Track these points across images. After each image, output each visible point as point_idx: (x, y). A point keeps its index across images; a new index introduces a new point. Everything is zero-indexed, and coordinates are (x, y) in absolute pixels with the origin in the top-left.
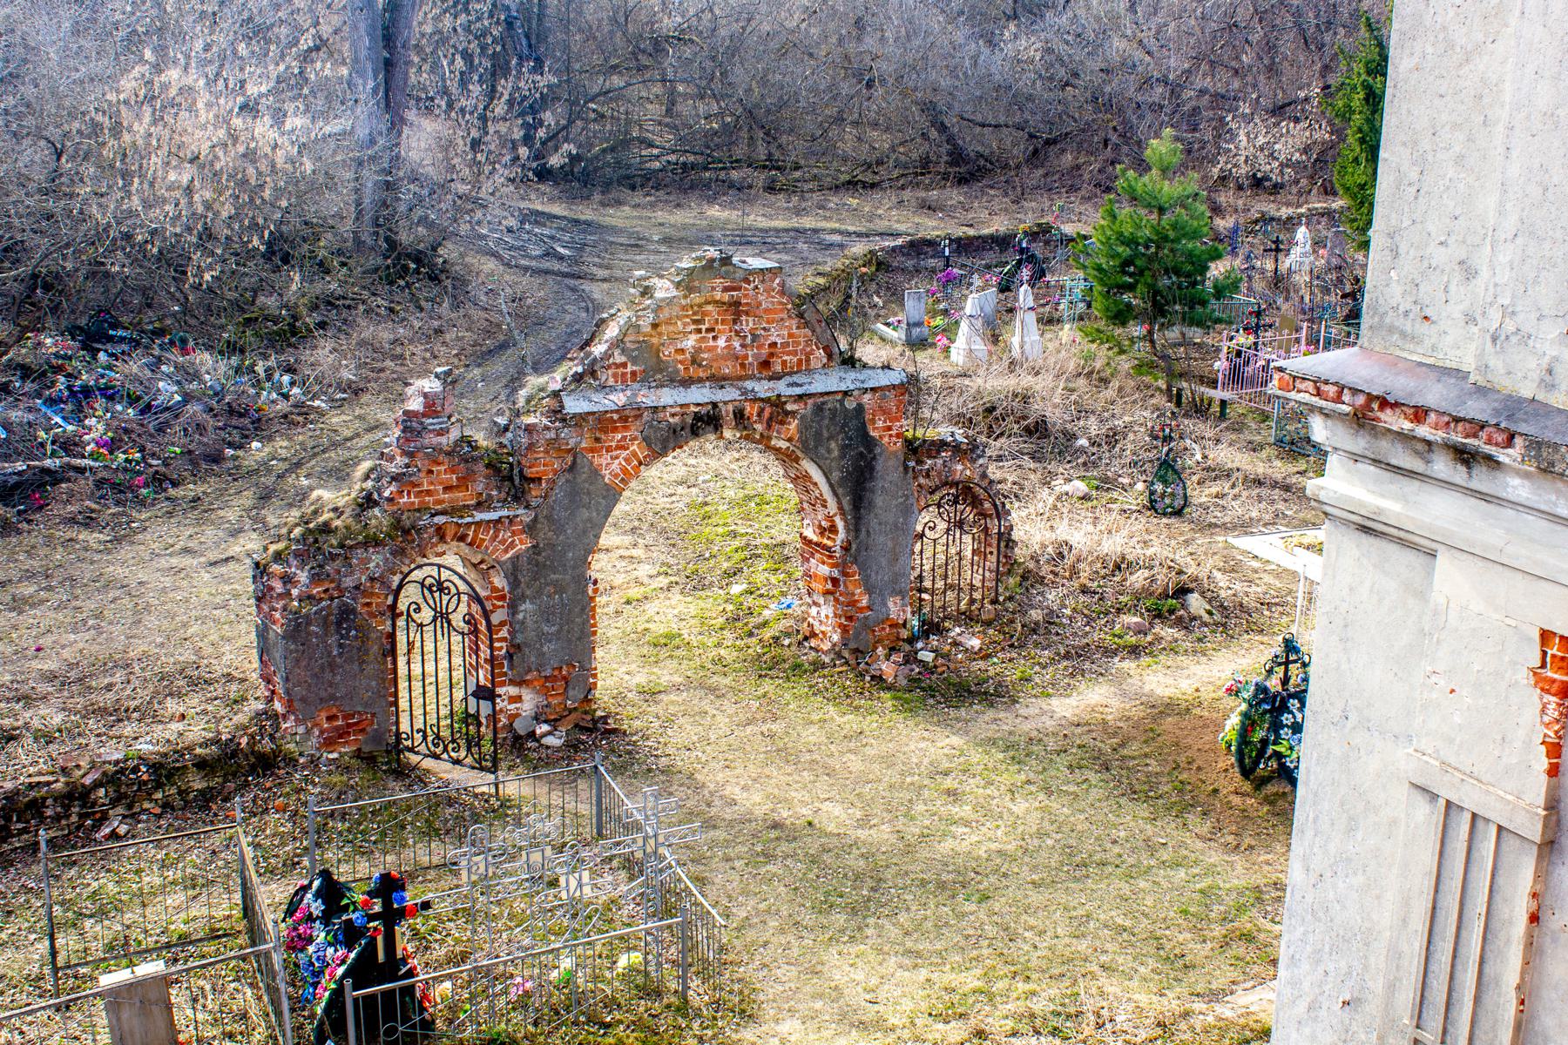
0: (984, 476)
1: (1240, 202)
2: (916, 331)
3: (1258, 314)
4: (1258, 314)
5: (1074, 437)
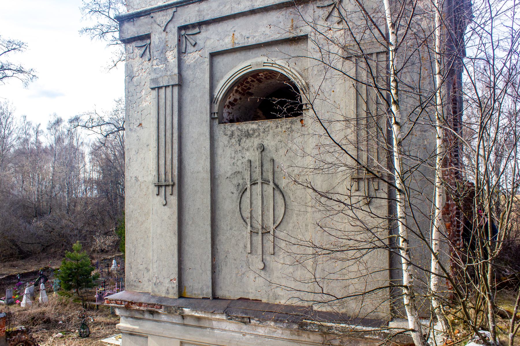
0: (31, 337)
1: (98, 256)
2: (10, 300)
3: (105, 282)
4: (105, 282)
5: (58, 321)
